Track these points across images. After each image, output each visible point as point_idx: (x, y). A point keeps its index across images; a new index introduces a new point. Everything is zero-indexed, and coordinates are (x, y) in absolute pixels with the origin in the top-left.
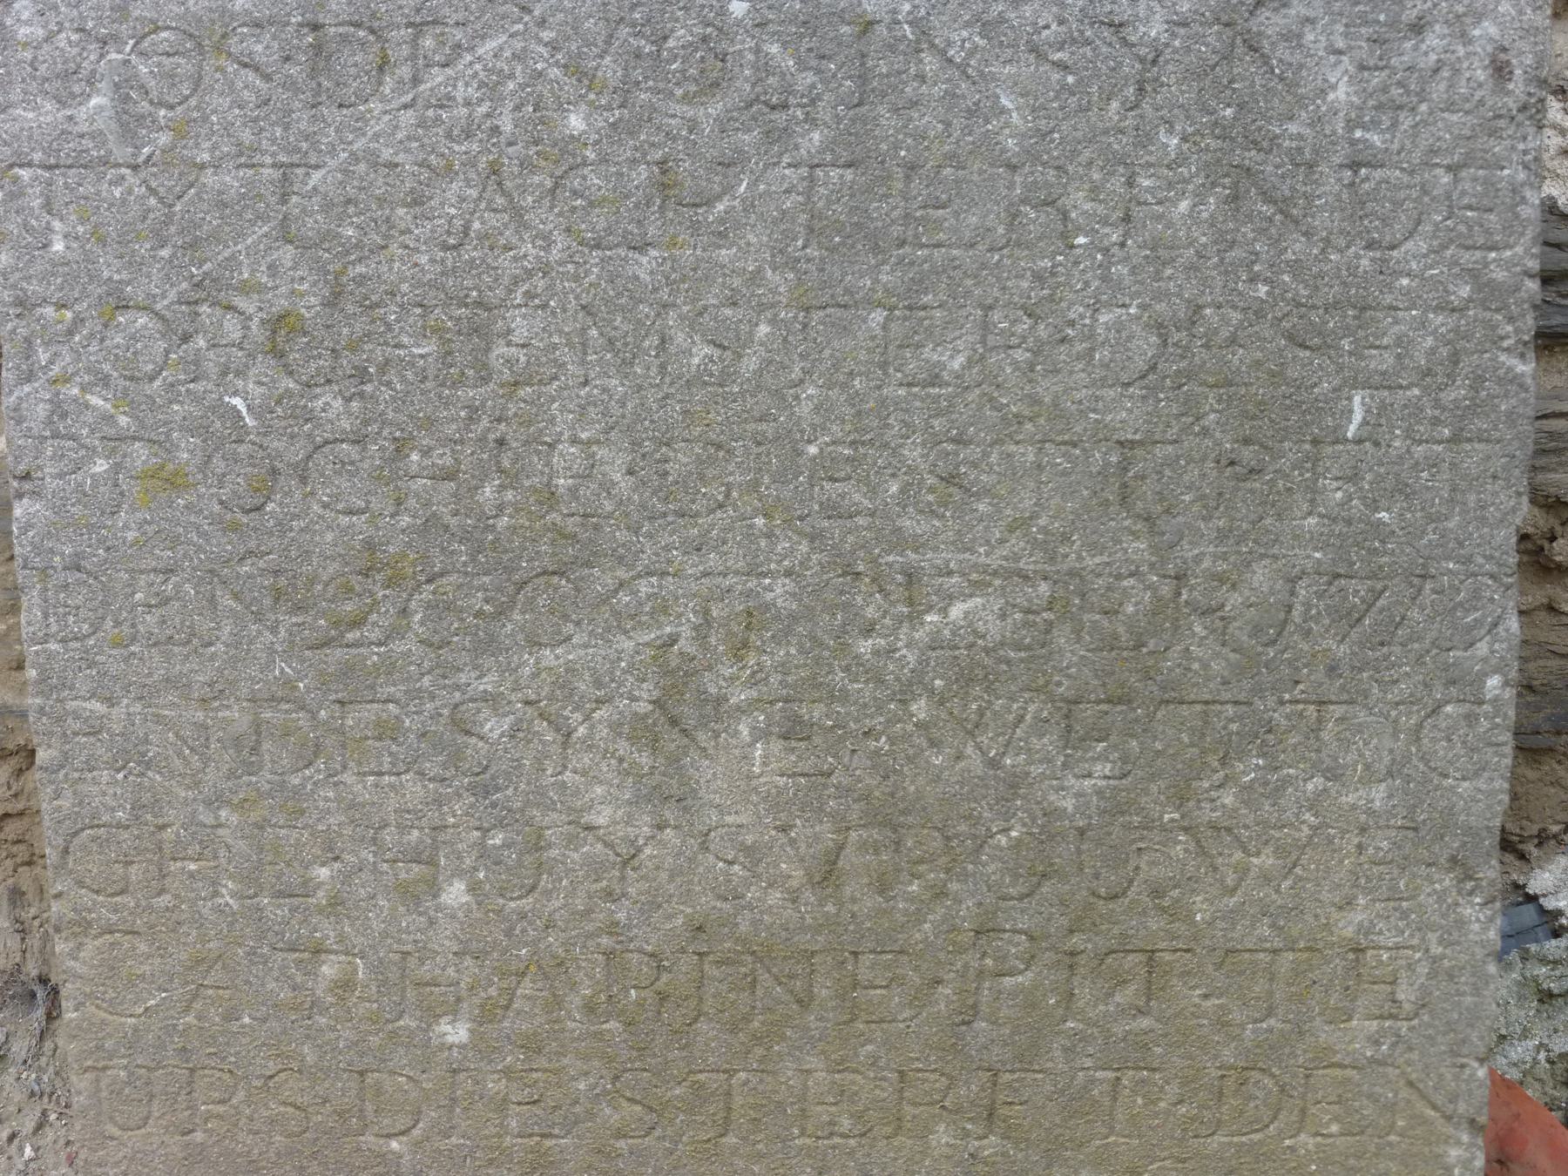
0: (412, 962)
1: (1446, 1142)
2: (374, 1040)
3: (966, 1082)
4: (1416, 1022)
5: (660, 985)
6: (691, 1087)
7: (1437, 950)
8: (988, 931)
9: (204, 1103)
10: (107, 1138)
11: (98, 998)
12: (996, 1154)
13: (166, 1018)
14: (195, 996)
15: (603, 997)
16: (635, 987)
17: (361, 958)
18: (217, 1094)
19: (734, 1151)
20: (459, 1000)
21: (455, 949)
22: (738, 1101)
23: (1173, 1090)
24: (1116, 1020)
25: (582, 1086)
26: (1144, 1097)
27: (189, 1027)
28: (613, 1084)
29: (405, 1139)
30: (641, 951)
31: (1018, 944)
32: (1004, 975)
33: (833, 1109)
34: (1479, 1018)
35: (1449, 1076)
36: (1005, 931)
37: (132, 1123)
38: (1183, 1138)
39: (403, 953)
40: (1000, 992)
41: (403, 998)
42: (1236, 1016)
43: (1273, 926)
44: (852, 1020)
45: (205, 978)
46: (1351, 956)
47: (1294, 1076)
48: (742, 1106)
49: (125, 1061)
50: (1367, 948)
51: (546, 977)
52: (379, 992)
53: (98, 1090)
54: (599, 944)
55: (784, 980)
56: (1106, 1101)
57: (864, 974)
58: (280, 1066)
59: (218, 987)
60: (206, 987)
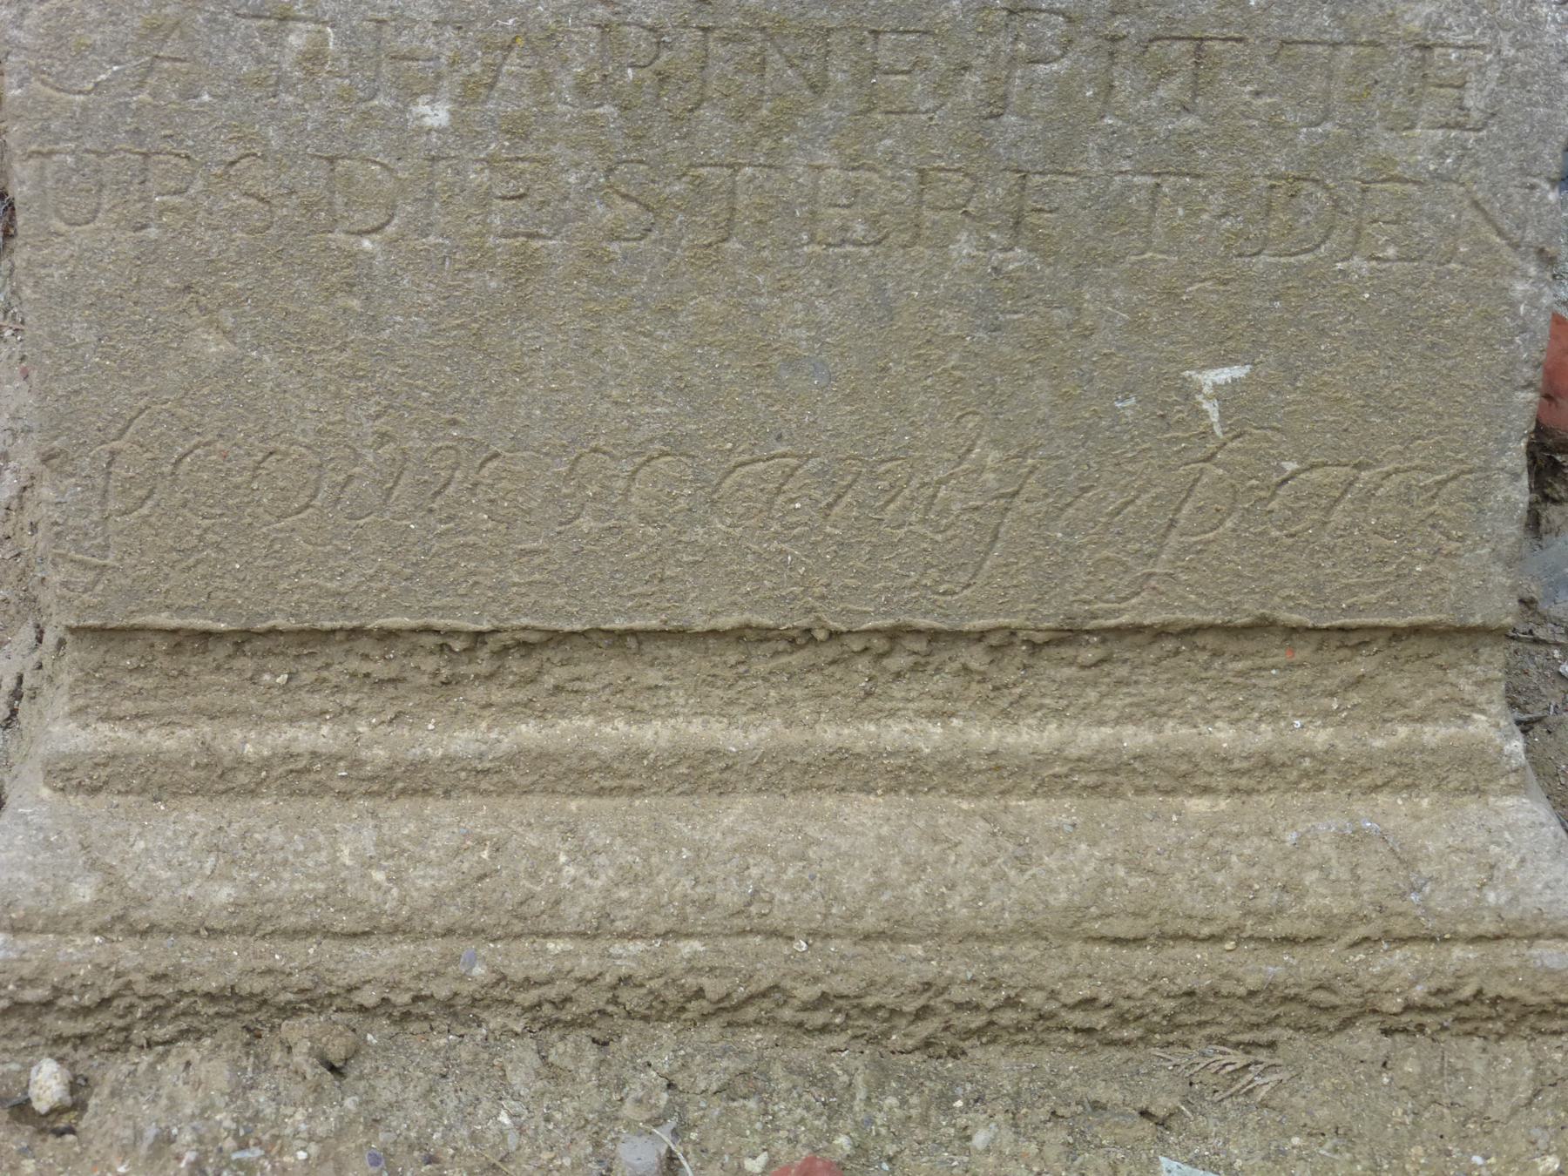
0: (388, 31)
1: (1511, 274)
2: (346, 122)
3: (992, 184)
4: (1484, 133)
5: (659, 64)
6: (691, 183)
7: (1509, 52)
8: (1023, 10)
9: (159, 194)
10: (52, 234)
11: (43, 72)
12: (1021, 269)
13: (118, 95)
14: (150, 69)
15: (597, 77)
16: (632, 66)
17: (332, 27)
18: (172, 184)
19: (737, 258)
20: (439, 77)
21: (435, 17)
22: (743, 200)
23: (1217, 201)
24: (1158, 118)
25: (572, 180)
26: (1185, 208)
27: (142, 105)
28: (607, 177)
29: (377, 237)
30: (640, 25)
31: (1055, 26)
32: (1038, 62)
33: (845, 212)
34: (1552, 132)
35: (1518, 198)
36: (1041, 11)
37: (79, 218)
38: (1226, 256)
39: (378, 21)
40: (1033, 81)
41: (378, 74)
42: (1290, 118)
43: (1333, 15)
44: (869, 110)
45: (160, 49)
46: (1417, 53)
47: (1350, 189)
48: (747, 206)
49: (72, 145)
50: (1435, 45)
51: (535, 52)
52: (351, 66)
53: (43, 179)
54: (593, 15)
55: (796, 61)
56: (1144, 210)
57: (885, 57)
58: (242, 151)
59: (176, 60)
60: (162, 59)
